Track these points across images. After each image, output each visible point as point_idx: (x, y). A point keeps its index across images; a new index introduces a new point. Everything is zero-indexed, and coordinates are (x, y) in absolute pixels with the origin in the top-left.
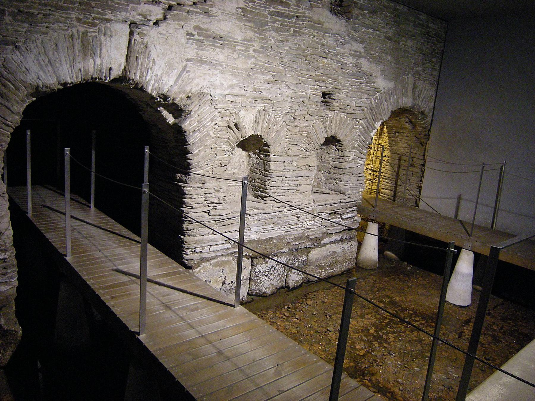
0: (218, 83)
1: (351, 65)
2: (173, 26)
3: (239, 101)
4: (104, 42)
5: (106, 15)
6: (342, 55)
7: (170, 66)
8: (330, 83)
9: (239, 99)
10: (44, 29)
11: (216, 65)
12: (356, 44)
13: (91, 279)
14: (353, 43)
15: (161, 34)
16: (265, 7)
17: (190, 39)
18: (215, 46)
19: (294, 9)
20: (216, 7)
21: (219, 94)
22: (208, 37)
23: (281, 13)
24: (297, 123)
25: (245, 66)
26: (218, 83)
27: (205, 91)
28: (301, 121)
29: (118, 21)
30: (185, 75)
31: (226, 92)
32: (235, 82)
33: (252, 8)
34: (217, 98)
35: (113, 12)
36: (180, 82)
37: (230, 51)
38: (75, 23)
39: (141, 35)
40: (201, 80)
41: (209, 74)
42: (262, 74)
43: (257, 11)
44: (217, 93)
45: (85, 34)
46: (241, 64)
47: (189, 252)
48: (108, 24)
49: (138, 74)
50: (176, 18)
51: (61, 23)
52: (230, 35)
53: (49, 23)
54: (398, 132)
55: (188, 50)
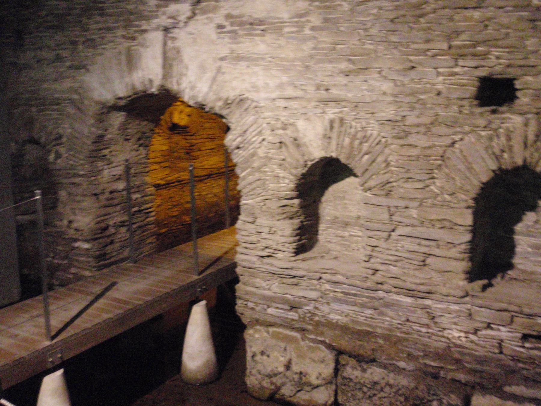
0: (260, 83)
3: (296, 106)
5: (140, 26)
7: (203, 68)
9: (294, 104)
11: (256, 59)
13: (495, 353)
22: (242, 24)
24: (411, 140)
25: (299, 55)
27: (247, 95)
30: (220, 78)
31: (274, 95)
32: (285, 79)
34: (262, 105)
37: (274, 36)
39: (174, 39)
40: (238, 82)
42: (330, 61)
44: (261, 97)
46: (289, 51)
47: (239, 302)
52: (272, 15)
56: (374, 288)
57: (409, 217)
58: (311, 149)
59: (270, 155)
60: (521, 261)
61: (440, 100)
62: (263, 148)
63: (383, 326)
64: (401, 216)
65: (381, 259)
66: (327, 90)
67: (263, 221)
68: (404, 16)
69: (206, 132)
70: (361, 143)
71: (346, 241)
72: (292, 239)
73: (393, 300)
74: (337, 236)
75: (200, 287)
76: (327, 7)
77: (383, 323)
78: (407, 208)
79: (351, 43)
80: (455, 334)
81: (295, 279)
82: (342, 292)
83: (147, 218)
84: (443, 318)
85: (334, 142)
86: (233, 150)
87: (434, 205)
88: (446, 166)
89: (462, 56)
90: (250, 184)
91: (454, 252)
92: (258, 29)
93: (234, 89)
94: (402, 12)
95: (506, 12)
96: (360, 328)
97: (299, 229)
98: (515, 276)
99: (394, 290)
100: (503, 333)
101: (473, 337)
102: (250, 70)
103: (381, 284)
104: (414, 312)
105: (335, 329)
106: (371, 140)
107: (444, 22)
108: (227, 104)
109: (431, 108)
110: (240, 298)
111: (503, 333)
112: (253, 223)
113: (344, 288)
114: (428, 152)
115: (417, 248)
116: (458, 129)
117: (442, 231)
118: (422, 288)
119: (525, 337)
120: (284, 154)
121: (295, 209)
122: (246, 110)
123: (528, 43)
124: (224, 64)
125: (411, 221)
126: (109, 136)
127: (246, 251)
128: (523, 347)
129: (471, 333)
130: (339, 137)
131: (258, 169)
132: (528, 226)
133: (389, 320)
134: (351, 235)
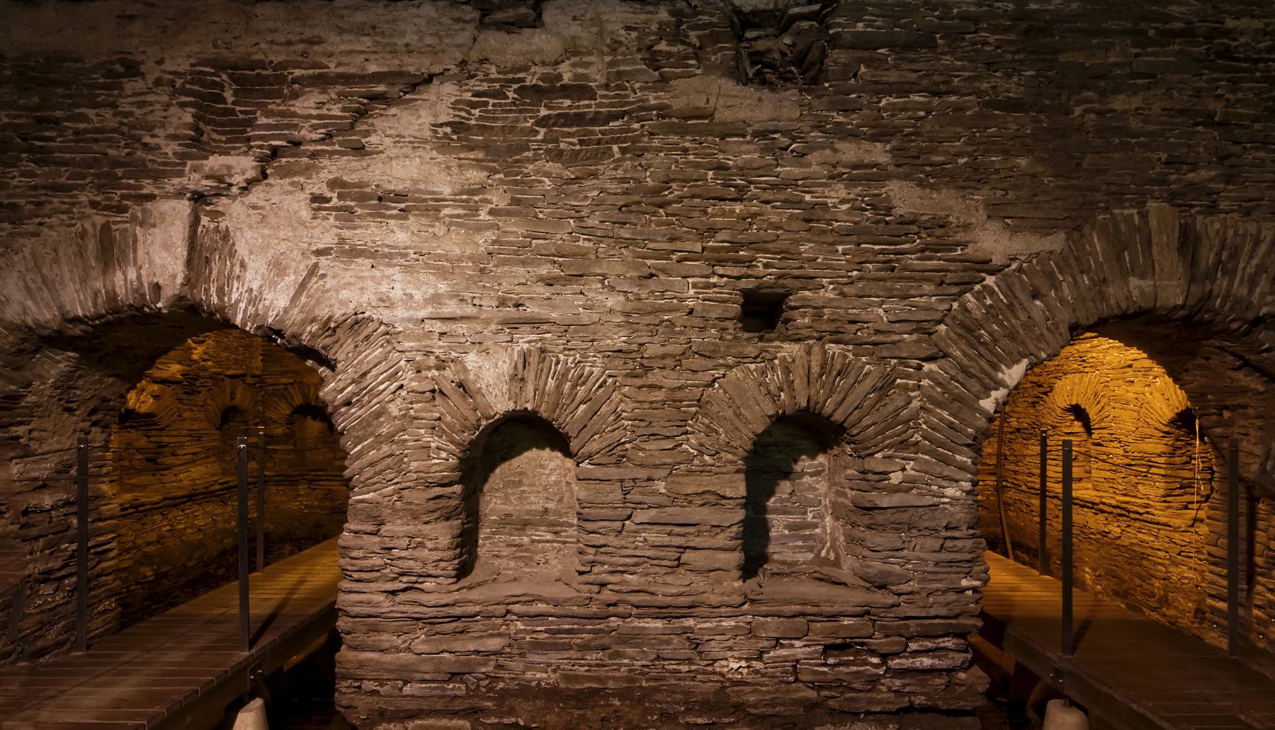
0: (397, 293)
1: (844, 207)
2: (278, 188)
3: (461, 332)
4: (140, 237)
5: (142, 187)
6: (809, 183)
7: (278, 267)
8: (766, 266)
9: (460, 328)
10: (31, 228)
12: (853, 146)
14: (840, 145)
15: (254, 207)
16: (520, 111)
17: (319, 209)
18: (383, 216)
19: (613, 97)
20: (380, 132)
21: (403, 320)
22: (362, 198)
23: (576, 115)
26: (397, 293)
28: (665, 373)
29: (167, 196)
30: (314, 284)
33: (480, 118)
34: (401, 329)
35: (155, 179)
36: (303, 299)
37: (424, 221)
38: (89, 211)
40: (349, 290)
41: (373, 278)
42: (524, 263)
43: (500, 124)
45: (106, 228)
46: (453, 244)
47: (343, 685)
48: (149, 205)
49: (213, 290)
50: (285, 173)
51: (63, 213)
52: (422, 187)
53: (43, 216)
54: (1226, 408)
55: (316, 232)
56: (604, 615)
57: (656, 493)
58: (491, 399)
59: (412, 412)
60: (777, 549)
61: (697, 321)
62: (399, 401)
63: (617, 674)
64: (641, 493)
65: (611, 565)
66: (517, 305)
67: (396, 527)
68: (638, 203)
69: (187, 425)
70: (574, 386)
71: (527, 550)
72: (450, 553)
73: (634, 628)
74: (508, 546)
75: (252, 672)
76: (516, 183)
77: (619, 670)
78: (649, 480)
79: (559, 236)
80: (733, 665)
81: (460, 622)
82: (546, 632)
83: (99, 563)
84: (713, 643)
85: (530, 388)
86: (337, 408)
87: (690, 472)
88: (705, 415)
89: (720, 262)
90: (372, 464)
91: (722, 540)
92: (395, 208)
93: (343, 303)
94: (636, 198)
95: (773, 207)
96: (578, 687)
97: (460, 535)
98: (775, 570)
99: (635, 611)
100: (799, 649)
101: (758, 665)
102: (377, 273)
103: (614, 605)
104: (668, 642)
105: (536, 698)
106: (592, 380)
107: (697, 214)
108: (329, 328)
109: (681, 333)
110: (345, 678)
111: (799, 649)
112: (375, 534)
113: (552, 622)
114: (679, 395)
115: (667, 540)
116: (721, 361)
117: (706, 510)
118: (682, 600)
119: (828, 650)
120: (440, 407)
121: (454, 502)
122: (367, 338)
123: (802, 248)
124: (323, 261)
125: (656, 500)
126: (32, 399)
127: (355, 586)
128: (825, 665)
129: (756, 659)
130: (537, 377)
131: (390, 439)
132: (782, 500)
133: (633, 659)
134: (533, 541)
